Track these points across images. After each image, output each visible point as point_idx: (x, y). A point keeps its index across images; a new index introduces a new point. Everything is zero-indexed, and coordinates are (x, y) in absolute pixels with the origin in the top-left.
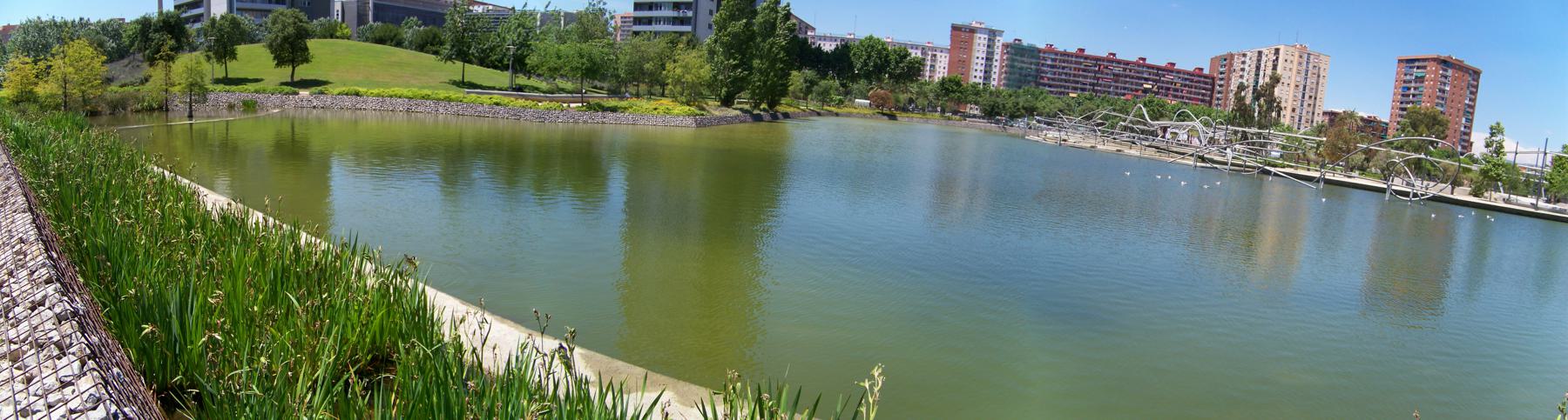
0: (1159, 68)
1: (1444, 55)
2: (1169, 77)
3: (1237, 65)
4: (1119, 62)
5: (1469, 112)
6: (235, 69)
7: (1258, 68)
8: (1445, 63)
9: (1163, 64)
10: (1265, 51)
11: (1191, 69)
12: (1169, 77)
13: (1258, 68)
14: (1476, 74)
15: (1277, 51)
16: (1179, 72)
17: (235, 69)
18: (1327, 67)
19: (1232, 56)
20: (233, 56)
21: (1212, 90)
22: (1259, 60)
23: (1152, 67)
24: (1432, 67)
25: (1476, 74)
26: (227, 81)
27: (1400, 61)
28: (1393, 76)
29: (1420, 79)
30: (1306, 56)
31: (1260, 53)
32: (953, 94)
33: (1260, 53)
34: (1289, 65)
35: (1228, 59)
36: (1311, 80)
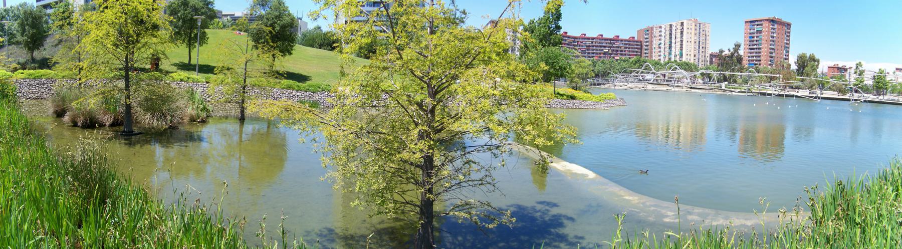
0: (611, 40)
1: (771, 17)
2: (617, 44)
3: (656, 32)
4: (588, 38)
5: (787, 47)
6: (203, 55)
7: (671, 34)
8: (772, 21)
9: (612, 37)
10: (674, 24)
11: (627, 38)
12: (617, 44)
13: (671, 34)
14: (788, 25)
15: (682, 24)
16: (622, 40)
17: (203, 55)
18: (710, 30)
19: (652, 28)
20: (203, 39)
21: (641, 49)
22: (671, 30)
23: (607, 39)
24: (766, 24)
25: (788, 25)
26: (187, 67)
27: (746, 22)
28: (743, 31)
29: (760, 32)
30: (698, 25)
31: (671, 26)
32: (860, 88)
33: (671, 26)
34: (690, 31)
35: (649, 31)
36: (702, 38)
